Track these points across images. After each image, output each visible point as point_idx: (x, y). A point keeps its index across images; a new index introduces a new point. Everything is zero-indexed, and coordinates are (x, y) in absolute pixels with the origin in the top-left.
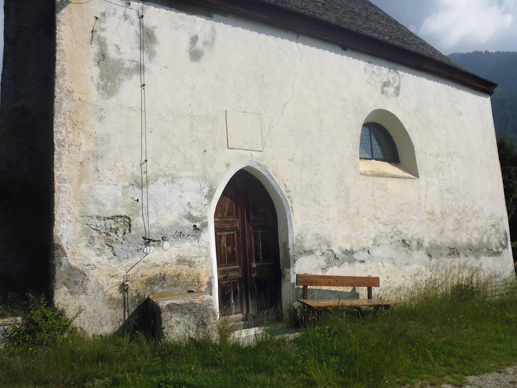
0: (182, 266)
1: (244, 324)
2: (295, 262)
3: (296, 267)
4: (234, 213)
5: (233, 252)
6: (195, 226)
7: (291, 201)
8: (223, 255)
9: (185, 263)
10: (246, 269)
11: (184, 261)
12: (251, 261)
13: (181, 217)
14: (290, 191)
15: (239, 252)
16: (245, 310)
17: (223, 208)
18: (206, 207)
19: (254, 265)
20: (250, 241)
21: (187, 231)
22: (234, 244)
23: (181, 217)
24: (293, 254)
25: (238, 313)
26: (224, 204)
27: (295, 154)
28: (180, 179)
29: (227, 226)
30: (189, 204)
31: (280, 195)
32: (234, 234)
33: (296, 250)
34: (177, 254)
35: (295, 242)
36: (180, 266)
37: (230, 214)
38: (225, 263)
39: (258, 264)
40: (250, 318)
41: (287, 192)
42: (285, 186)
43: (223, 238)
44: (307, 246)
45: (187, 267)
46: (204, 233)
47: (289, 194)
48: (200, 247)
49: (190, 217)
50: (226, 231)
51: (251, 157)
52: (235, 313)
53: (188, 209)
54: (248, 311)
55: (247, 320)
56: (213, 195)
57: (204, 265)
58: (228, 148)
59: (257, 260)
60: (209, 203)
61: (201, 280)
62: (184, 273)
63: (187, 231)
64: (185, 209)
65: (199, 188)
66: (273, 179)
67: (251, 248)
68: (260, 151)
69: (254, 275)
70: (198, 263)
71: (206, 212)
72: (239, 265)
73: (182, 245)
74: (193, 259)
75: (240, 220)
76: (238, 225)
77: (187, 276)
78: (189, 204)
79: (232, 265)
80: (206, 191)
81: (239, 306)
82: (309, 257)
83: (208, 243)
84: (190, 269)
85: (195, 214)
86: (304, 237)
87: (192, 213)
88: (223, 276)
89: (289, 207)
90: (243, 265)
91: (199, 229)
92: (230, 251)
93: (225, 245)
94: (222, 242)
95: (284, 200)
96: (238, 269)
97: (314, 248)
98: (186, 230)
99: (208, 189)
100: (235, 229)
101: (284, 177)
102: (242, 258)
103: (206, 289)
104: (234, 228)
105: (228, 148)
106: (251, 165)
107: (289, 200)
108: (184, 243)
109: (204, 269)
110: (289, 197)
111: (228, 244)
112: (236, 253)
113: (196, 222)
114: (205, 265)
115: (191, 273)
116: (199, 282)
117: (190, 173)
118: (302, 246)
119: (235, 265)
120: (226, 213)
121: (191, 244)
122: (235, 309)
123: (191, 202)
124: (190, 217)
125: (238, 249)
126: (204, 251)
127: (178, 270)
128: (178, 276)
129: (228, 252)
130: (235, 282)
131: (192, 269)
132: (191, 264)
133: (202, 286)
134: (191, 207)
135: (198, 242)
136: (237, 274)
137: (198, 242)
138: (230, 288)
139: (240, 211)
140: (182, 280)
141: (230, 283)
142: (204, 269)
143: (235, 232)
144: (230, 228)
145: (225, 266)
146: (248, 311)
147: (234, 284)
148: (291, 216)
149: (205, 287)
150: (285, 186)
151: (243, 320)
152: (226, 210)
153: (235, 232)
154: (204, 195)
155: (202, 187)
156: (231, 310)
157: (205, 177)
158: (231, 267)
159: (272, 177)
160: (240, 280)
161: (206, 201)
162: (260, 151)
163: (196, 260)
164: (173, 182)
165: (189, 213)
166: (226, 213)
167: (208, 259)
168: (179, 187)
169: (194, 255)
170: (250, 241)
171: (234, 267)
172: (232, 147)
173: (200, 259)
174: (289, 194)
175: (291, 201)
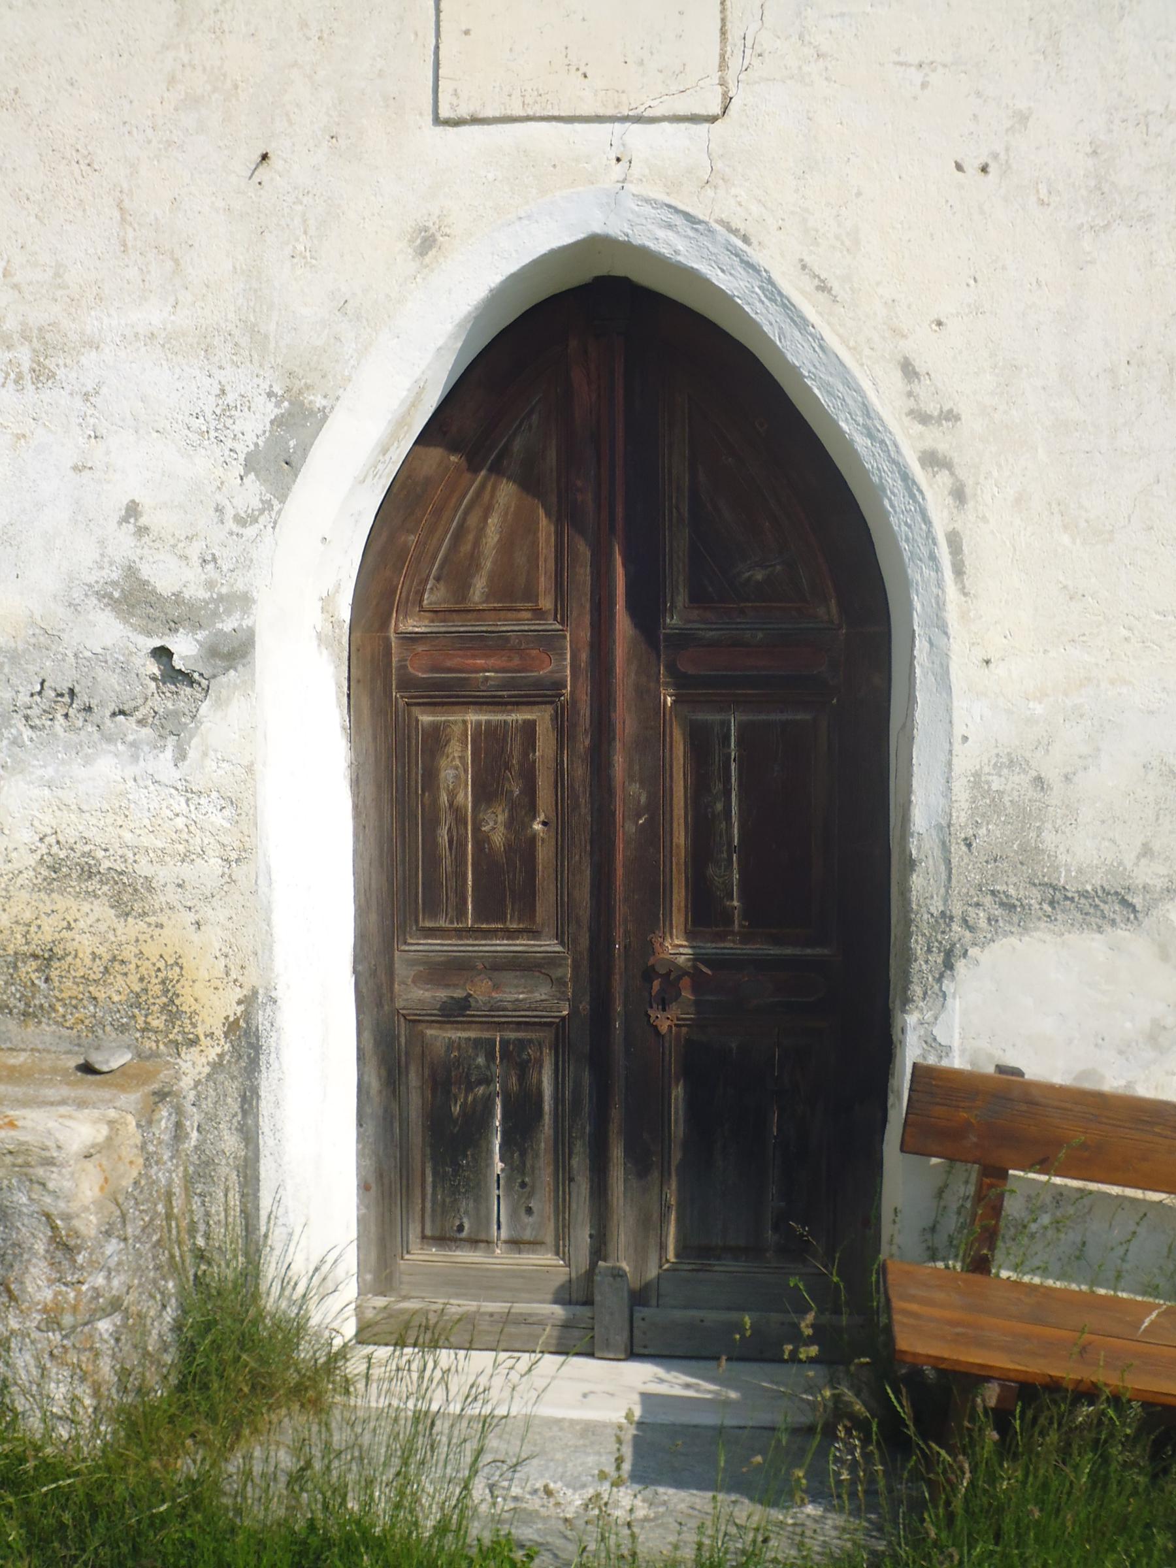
0: (71, 902)
1: (566, 1326)
2: (949, 965)
3: (955, 1005)
4: (544, 582)
5: (523, 848)
6: (162, 654)
7: (959, 495)
8: (447, 864)
9: (93, 885)
10: (604, 965)
11: (88, 873)
12: (651, 918)
13: (77, 595)
14: (951, 416)
15: (560, 852)
16: (582, 1236)
17: (466, 548)
18: (250, 531)
19: (676, 947)
20: (655, 779)
21: (110, 686)
22: (530, 790)
23: (77, 595)
24: (937, 906)
25: (535, 1244)
26: (473, 521)
27: (1023, 118)
28: (89, 358)
29: (487, 670)
30: (132, 511)
31: (861, 443)
32: (529, 728)
33: (967, 869)
34: (47, 821)
35: (961, 817)
36: (62, 902)
37: (511, 591)
38: (461, 913)
39: (710, 948)
40: (611, 1301)
41: (924, 418)
42: (909, 370)
43: (454, 749)
44: (1081, 850)
45: (102, 910)
46: (219, 703)
47: (938, 439)
48: (189, 793)
49: (133, 598)
50: (479, 703)
51: (618, 171)
52: (515, 1244)
53: (123, 544)
54: (599, 1248)
55: (588, 1302)
56: (305, 449)
57: (216, 914)
58: (438, 121)
59: (705, 915)
60: (267, 506)
61: (186, 1003)
62: (85, 944)
63: (110, 686)
64: (102, 543)
65: (209, 404)
66: (801, 323)
67: (653, 835)
68: (694, 119)
69: (664, 1021)
70: (171, 895)
71: (245, 563)
72: (559, 937)
73: (78, 771)
74: (144, 868)
75: (585, 634)
76: (565, 667)
77: (98, 966)
78: (132, 511)
79: (511, 934)
80: (253, 426)
81: (542, 1203)
82: (1092, 946)
83: (250, 769)
84: (120, 926)
85: (168, 576)
86: (1052, 776)
87: (146, 572)
88: (442, 994)
89: (930, 538)
90: (584, 942)
91: (186, 678)
92: (498, 838)
93: (466, 798)
94: (447, 774)
95: (892, 482)
96: (552, 961)
97: (1149, 874)
98: (100, 674)
99: (271, 410)
100: (544, 693)
101: (881, 307)
102: (583, 895)
103: (217, 1066)
104: (538, 684)
105: (438, 121)
106: (616, 228)
107: (934, 492)
108: (88, 761)
109: (213, 938)
110: (932, 460)
111: (485, 793)
112: (544, 854)
113: (173, 625)
114: (221, 915)
115: (129, 953)
116: (172, 1013)
117: (153, 315)
118: (1031, 853)
119: (534, 934)
120: (479, 586)
121: (130, 771)
122: (514, 1215)
123: (146, 501)
124: (133, 598)
125: (561, 824)
126: (218, 820)
127: (46, 922)
128: (47, 959)
129: (481, 841)
130: (522, 1044)
131: (133, 927)
132: (128, 894)
133: (194, 1042)
134: (142, 531)
135: (181, 756)
136: (542, 993)
137: (181, 756)
138: (488, 1081)
139: (584, 574)
140: (70, 989)
141: (486, 1046)
142: (213, 938)
143: (541, 717)
144: (506, 685)
145: (460, 933)
146: (599, 1248)
147: (518, 1059)
148: (940, 605)
149: (213, 1054)
150: (909, 370)
151: (563, 1297)
152: (488, 565)
153: (541, 717)
154: (242, 450)
155: (231, 398)
156: (482, 1221)
157: (252, 330)
158: (501, 946)
159: (788, 306)
160: (560, 1032)
161: (251, 493)
162: (694, 119)
163: (164, 874)
164: (41, 375)
165: (131, 571)
166: (479, 586)
167: (238, 871)
168: (78, 402)
169: (147, 841)
170: (655, 779)
171: (520, 945)
172: (464, 112)
173: (186, 871)
174: (938, 439)
175: (959, 495)
